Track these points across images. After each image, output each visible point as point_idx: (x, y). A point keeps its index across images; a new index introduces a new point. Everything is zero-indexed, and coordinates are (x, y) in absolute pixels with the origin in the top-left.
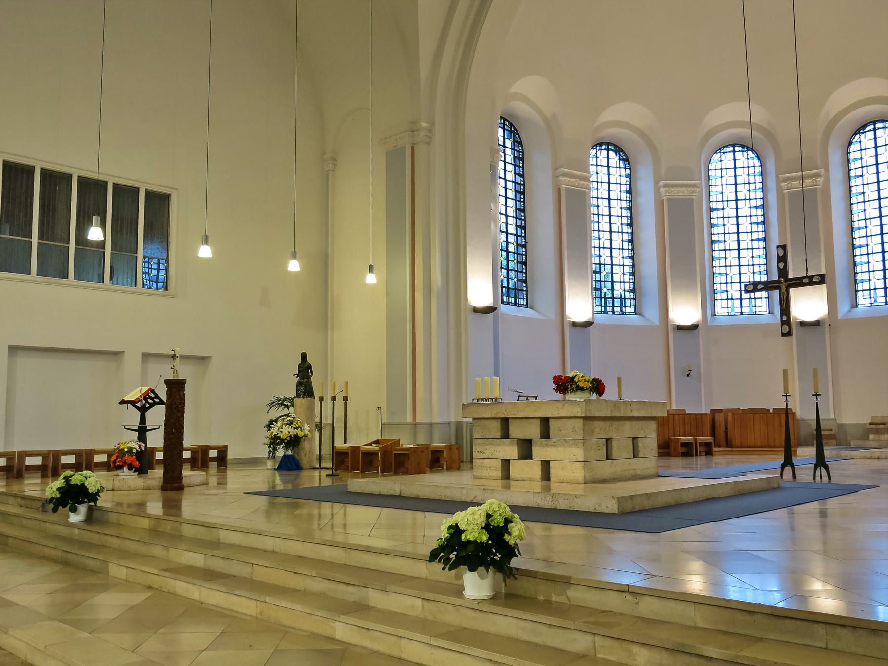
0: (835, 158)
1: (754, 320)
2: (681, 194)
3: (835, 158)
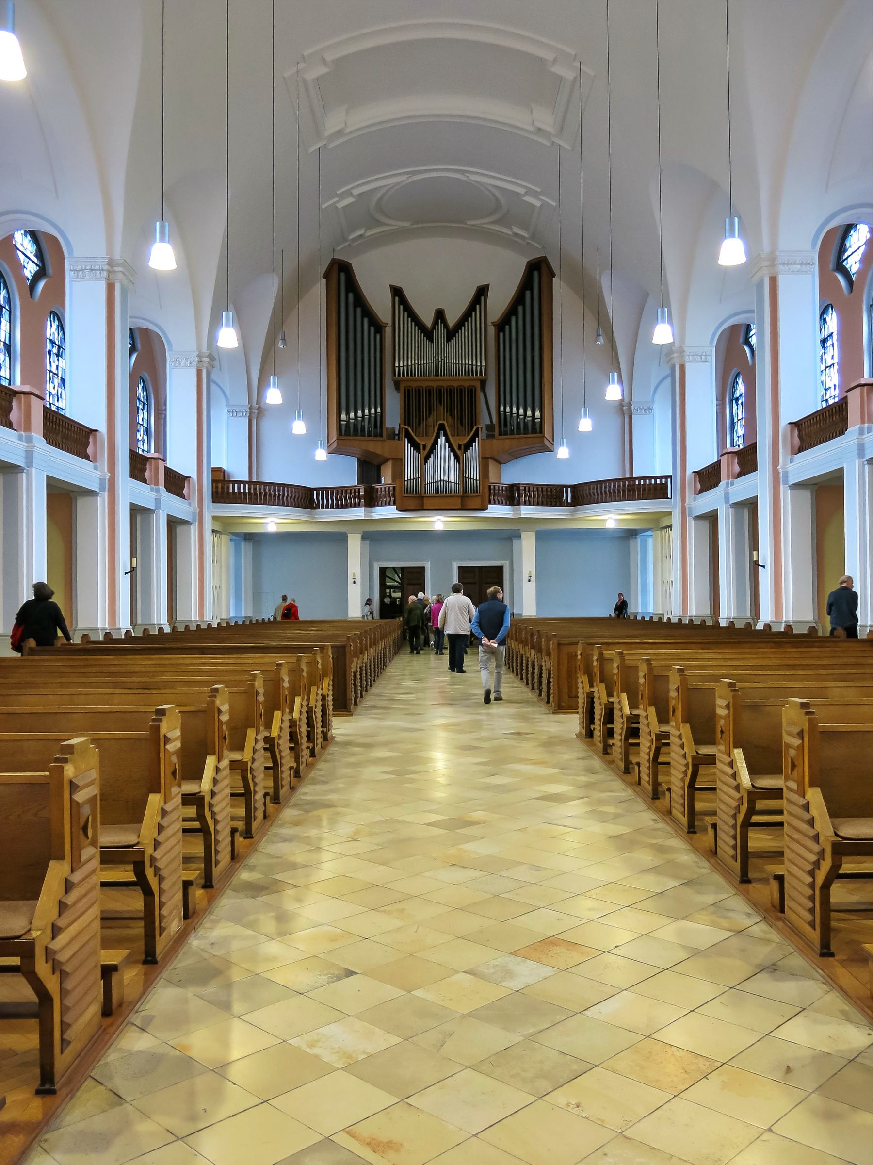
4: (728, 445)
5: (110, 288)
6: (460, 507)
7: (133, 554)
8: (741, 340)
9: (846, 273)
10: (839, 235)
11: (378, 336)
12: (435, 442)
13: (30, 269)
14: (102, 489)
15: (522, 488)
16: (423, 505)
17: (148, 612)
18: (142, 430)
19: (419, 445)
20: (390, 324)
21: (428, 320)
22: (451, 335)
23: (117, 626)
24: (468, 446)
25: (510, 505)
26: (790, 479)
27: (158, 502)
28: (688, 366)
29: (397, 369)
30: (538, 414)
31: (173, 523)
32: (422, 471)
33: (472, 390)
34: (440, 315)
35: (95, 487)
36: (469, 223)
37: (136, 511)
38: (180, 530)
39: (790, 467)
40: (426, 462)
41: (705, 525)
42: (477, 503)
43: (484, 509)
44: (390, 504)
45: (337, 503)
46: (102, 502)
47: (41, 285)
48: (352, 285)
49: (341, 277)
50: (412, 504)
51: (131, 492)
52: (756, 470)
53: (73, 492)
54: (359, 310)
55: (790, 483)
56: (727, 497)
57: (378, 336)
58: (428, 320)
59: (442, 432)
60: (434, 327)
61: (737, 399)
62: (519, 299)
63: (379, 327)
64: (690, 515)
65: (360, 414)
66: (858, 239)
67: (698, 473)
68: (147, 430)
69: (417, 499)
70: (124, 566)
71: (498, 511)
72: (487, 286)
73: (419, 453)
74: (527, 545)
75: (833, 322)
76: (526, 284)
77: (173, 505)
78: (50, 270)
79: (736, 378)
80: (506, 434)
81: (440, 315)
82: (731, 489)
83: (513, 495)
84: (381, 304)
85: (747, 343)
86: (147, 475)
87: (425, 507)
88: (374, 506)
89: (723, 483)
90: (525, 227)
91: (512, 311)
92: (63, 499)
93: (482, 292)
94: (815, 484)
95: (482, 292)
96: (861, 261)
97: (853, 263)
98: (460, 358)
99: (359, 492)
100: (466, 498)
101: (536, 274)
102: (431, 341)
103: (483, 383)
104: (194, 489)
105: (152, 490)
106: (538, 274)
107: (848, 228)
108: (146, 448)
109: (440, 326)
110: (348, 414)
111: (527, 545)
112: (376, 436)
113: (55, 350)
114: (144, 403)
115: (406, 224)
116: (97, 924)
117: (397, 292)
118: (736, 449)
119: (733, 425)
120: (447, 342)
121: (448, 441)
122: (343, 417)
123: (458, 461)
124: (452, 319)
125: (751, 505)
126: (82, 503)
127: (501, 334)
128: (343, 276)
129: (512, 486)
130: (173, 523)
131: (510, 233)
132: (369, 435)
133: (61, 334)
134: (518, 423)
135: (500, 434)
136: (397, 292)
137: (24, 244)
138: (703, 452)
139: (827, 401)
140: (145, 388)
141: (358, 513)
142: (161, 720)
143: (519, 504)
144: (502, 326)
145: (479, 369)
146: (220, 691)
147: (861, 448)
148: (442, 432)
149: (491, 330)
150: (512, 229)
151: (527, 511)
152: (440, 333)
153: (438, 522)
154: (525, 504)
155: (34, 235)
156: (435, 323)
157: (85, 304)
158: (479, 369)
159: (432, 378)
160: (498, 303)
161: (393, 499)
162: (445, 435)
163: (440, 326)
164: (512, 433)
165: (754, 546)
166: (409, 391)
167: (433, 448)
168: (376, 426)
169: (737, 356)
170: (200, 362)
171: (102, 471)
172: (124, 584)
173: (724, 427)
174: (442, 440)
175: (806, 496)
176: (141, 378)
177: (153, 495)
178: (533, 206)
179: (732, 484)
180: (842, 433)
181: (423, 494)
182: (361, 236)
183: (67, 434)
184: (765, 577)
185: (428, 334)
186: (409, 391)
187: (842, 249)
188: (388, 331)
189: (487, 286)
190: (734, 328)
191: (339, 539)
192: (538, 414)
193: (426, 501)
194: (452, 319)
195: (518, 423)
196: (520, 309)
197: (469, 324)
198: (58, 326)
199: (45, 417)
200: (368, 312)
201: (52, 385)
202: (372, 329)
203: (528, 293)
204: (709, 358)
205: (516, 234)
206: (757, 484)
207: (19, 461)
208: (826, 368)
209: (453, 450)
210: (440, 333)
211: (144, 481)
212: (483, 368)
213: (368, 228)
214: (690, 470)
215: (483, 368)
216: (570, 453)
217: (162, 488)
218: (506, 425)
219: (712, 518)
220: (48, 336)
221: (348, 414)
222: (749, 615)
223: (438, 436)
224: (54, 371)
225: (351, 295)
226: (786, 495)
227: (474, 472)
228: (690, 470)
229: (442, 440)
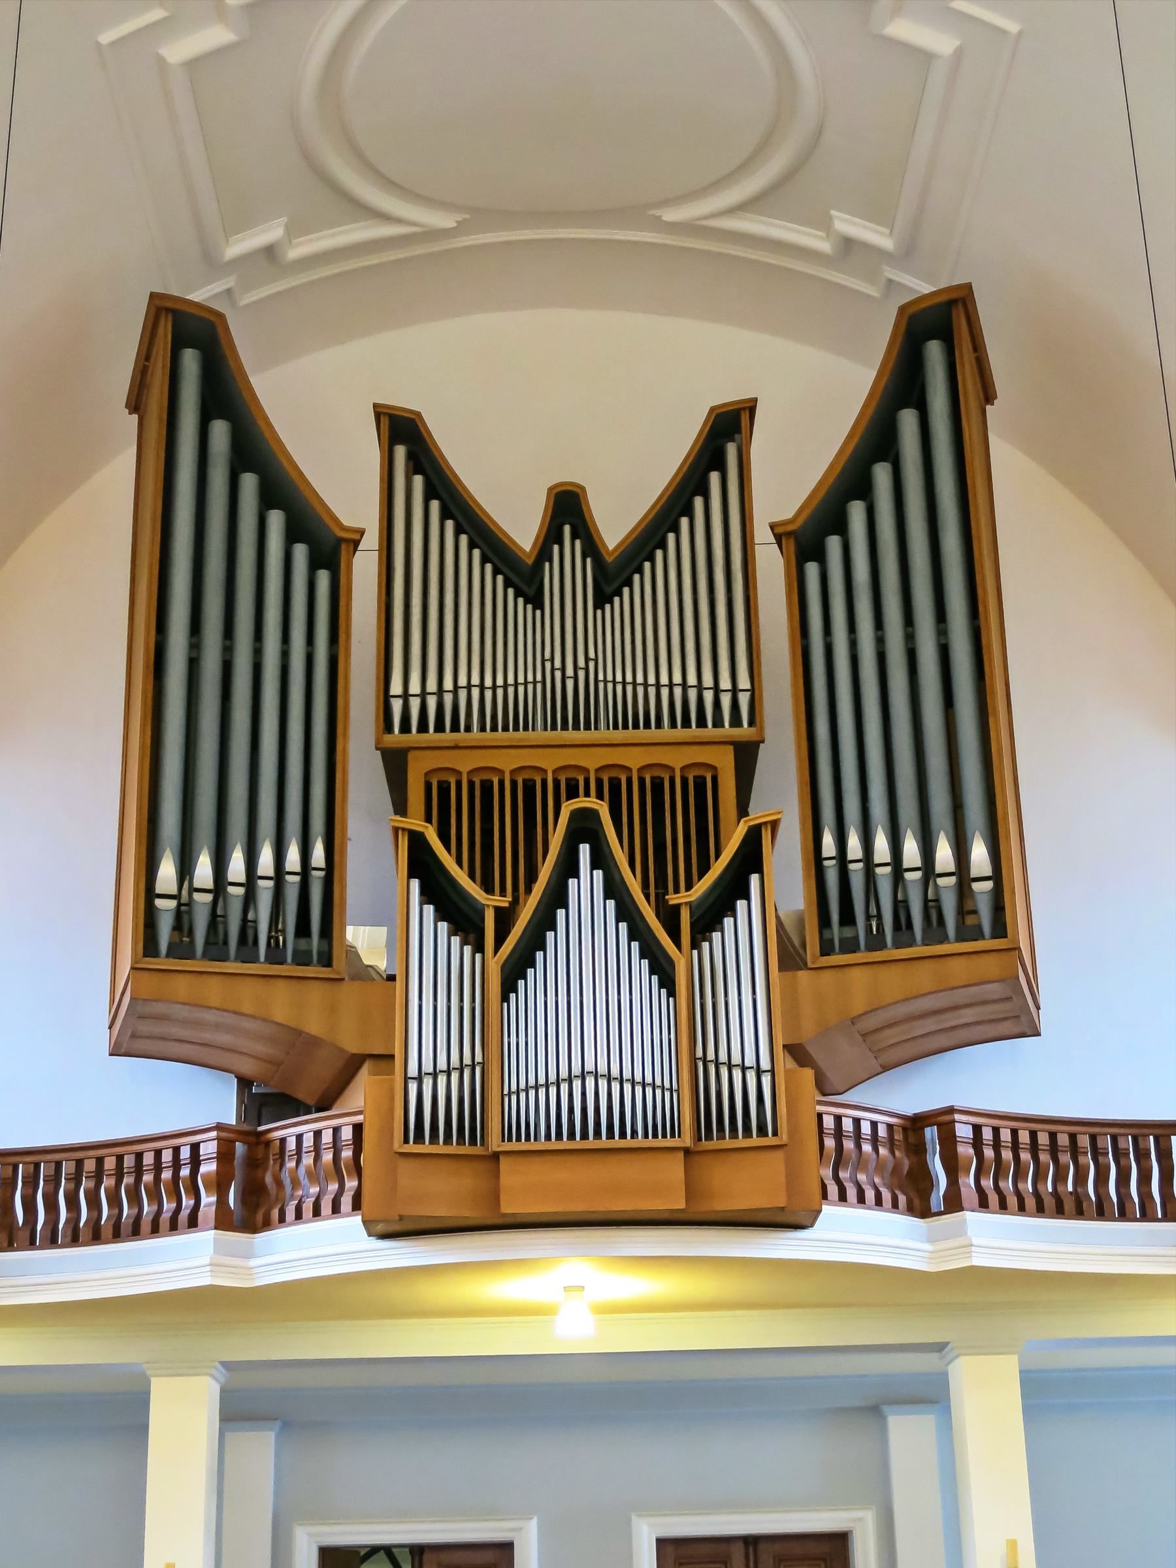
6: (677, 1203)
11: (323, 577)
12: (557, 897)
15: (963, 1131)
16: (495, 1197)
19: (479, 911)
20: (371, 541)
21: (522, 528)
22: (611, 578)
24: (711, 916)
25: (911, 1210)
29: (397, 706)
30: (979, 853)
32: (488, 1031)
33: (700, 784)
34: (567, 509)
36: (671, 215)
40: (509, 987)
42: (749, 1181)
43: (789, 1219)
44: (336, 1209)
45: (74, 1220)
48: (224, 395)
49: (191, 363)
50: (443, 1189)
54: (249, 483)
57: (323, 577)
58: (522, 528)
59: (585, 850)
60: (543, 554)
62: (876, 441)
63: (328, 550)
65: (236, 867)
69: (477, 1171)
71: (858, 1233)
72: (750, 407)
73: (479, 948)
74: (988, 1394)
76: (903, 385)
80: (850, 946)
81: (567, 509)
83: (920, 1167)
84: (346, 479)
87: (510, 1207)
88: (267, 1225)
90: (879, 214)
91: (850, 483)
93: (728, 427)
95: (728, 427)
98: (649, 650)
99: (195, 1161)
100: (702, 1163)
101: (934, 351)
102: (536, 601)
103: (746, 756)
106: (935, 345)
109: (570, 548)
110: (185, 869)
111: (988, 1394)
112: (302, 958)
115: (445, 221)
117: (402, 431)
120: (599, 604)
121: (614, 889)
122: (167, 871)
123: (668, 983)
124: (614, 527)
127: (812, 569)
128: (190, 360)
129: (915, 1124)
131: (825, 246)
132: (275, 955)
134: (901, 907)
135: (826, 948)
136: (402, 431)
141: (188, 1259)
143: (953, 1203)
144: (806, 542)
145: (726, 700)
148: (585, 850)
149: (771, 564)
150: (825, 224)
151: (997, 1239)
152: (569, 572)
153: (571, 1297)
154: (984, 1204)
156: (551, 536)
158: (726, 700)
159: (539, 735)
160: (786, 473)
161: (351, 1184)
162: (600, 859)
163: (570, 548)
164: (876, 942)
166: (444, 789)
167: (545, 922)
168: (303, 929)
174: (586, 885)
178: (926, 57)
181: (495, 1143)
182: (270, 252)
185: (524, 579)
186: (444, 789)
188: (364, 568)
189: (750, 407)
191: (115, 1416)
192: (979, 853)
193: (511, 1175)
194: (614, 527)
195: (901, 907)
196: (882, 474)
197: (684, 539)
200: (282, 491)
202: (300, 552)
203: (908, 419)
205: (848, 244)
209: (639, 932)
210: (569, 572)
212: (744, 699)
213: (295, 230)
215: (744, 699)
218: (848, 917)
221: (185, 869)
223: (568, 867)
225: (220, 430)
227: (746, 1030)
229: (586, 885)
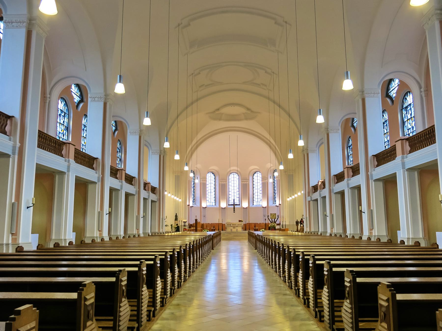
0: (251, 178)
1: (212, 207)
2: (204, 182)
3: (251, 178)
4: (401, 136)
5: (105, 104)
7: (110, 206)
8: (350, 125)
9: (391, 98)
10: (387, 82)
13: (77, 99)
14: (99, 181)
17: (116, 230)
18: (118, 159)
23: (61, 238)
26: (406, 166)
27: (122, 187)
28: (330, 135)
31: (152, 201)
35: (9, 152)
37: (112, 190)
38: (130, 198)
39: (334, 188)
41: (339, 196)
46: (136, 197)
47: (81, 105)
51: (110, 182)
52: (359, 174)
53: (54, 172)
55: (406, 168)
56: (348, 185)
61: (350, 147)
64: (372, 179)
66: (395, 84)
67: (335, 176)
68: (120, 160)
70: (106, 211)
75: (386, 117)
77: (128, 188)
78: (85, 100)
79: (405, 96)
82: (350, 182)
85: (353, 126)
86: (118, 176)
89: (346, 179)
92: (82, 185)
94: (419, 169)
96: (396, 93)
97: (393, 94)
104: (99, 165)
105: (66, 161)
107: (391, 81)
108: (120, 166)
113: (63, 114)
114: (65, 113)
116: (126, 328)
118: (350, 166)
119: (348, 156)
125: (358, 188)
126: (90, 187)
130: (127, 195)
133: (66, 108)
137: (74, 89)
138: (337, 167)
139: (409, 134)
140: (120, 144)
142: (120, 274)
146: (87, 286)
147: (403, 164)
155: (78, 86)
157: (95, 110)
165: (360, 204)
169: (350, 130)
170: (160, 153)
171: (99, 174)
172: (106, 218)
173: (345, 158)
175: (381, 184)
176: (119, 140)
177: (148, 194)
179: (407, 157)
180: (394, 159)
183: (87, 161)
184: (365, 217)
187: (388, 89)
190: (347, 120)
198: (65, 104)
199: (39, 136)
201: (84, 142)
204: (339, 131)
206: (359, 180)
207: (65, 170)
208: (408, 120)
211: (117, 178)
214: (311, 185)
216: (415, 8)
217: (150, 192)
219: (342, 193)
220: (83, 123)
222: (359, 233)
224: (62, 123)
226: (372, 184)
228: (311, 185)
